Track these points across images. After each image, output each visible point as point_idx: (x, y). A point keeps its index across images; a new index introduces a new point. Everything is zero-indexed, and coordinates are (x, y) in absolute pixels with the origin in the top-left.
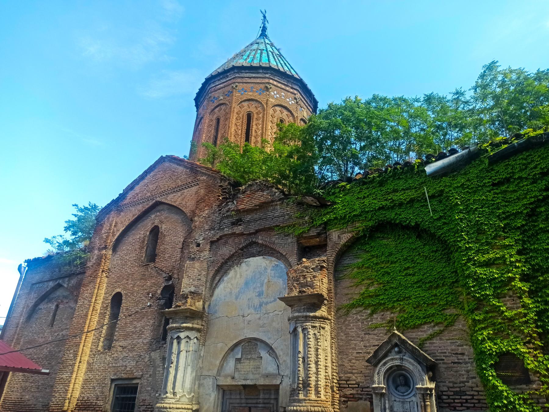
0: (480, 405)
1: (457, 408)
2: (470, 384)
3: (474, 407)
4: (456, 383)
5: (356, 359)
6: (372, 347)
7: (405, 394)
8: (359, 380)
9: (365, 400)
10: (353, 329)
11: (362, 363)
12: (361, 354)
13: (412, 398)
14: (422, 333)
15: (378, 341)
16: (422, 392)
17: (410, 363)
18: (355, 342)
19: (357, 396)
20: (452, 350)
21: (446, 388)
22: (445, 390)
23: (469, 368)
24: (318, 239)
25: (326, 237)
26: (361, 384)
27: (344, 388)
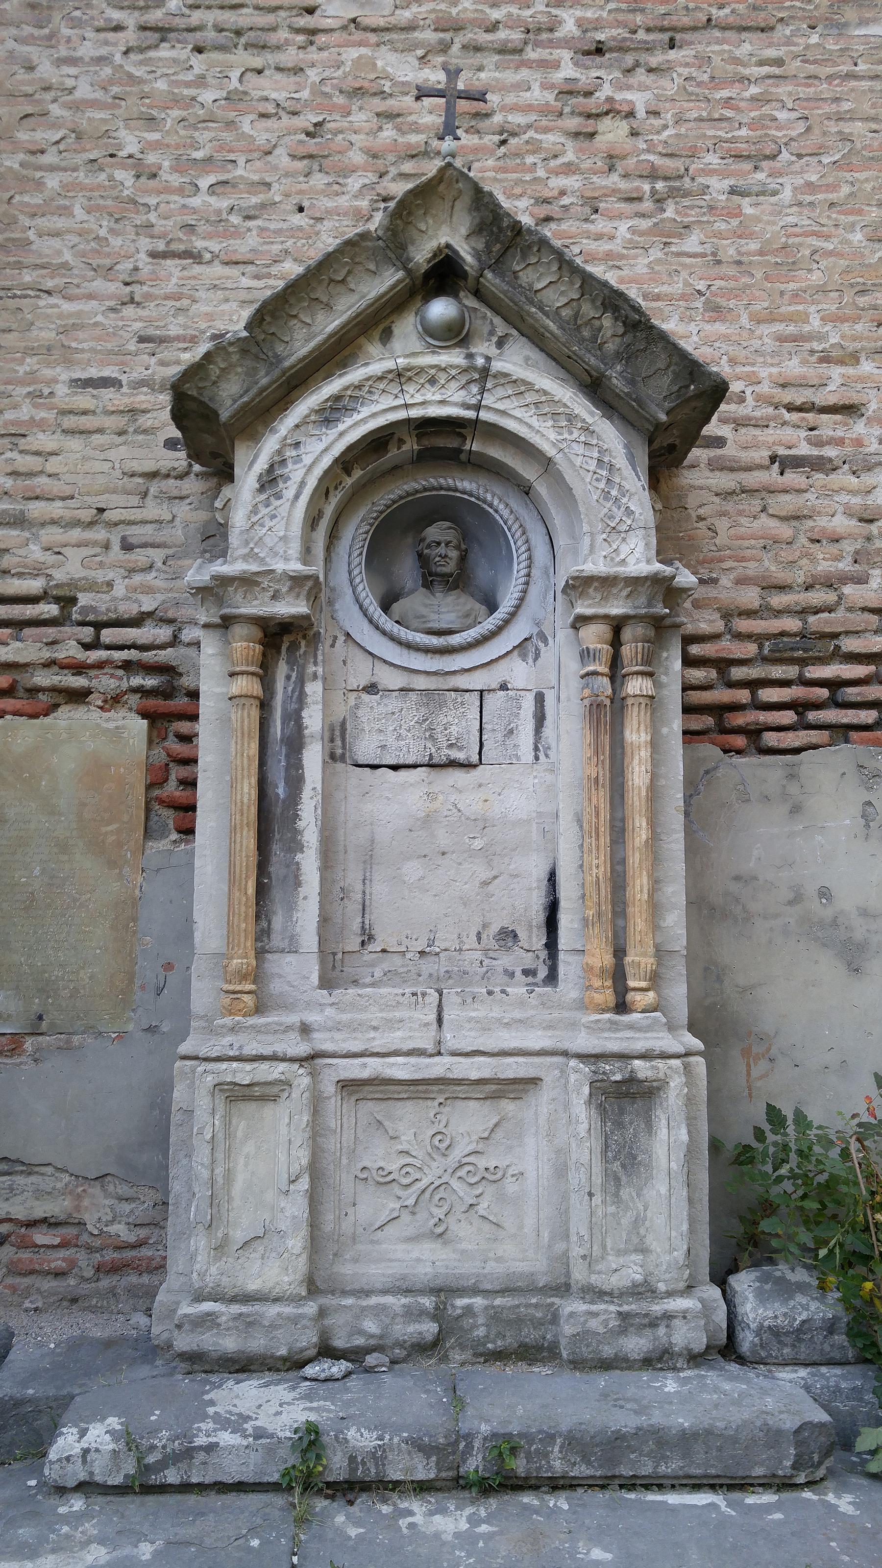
1: (771, 739)
4: (782, 588)
5: (70, 422)
7: (456, 640)
9: (114, 701)
10: (66, 211)
11: (112, 454)
12: (108, 394)
13: (503, 664)
18: (67, 307)
19: (43, 679)
20: (784, 386)
21: (717, 616)
22: (704, 627)
26: (84, 599)
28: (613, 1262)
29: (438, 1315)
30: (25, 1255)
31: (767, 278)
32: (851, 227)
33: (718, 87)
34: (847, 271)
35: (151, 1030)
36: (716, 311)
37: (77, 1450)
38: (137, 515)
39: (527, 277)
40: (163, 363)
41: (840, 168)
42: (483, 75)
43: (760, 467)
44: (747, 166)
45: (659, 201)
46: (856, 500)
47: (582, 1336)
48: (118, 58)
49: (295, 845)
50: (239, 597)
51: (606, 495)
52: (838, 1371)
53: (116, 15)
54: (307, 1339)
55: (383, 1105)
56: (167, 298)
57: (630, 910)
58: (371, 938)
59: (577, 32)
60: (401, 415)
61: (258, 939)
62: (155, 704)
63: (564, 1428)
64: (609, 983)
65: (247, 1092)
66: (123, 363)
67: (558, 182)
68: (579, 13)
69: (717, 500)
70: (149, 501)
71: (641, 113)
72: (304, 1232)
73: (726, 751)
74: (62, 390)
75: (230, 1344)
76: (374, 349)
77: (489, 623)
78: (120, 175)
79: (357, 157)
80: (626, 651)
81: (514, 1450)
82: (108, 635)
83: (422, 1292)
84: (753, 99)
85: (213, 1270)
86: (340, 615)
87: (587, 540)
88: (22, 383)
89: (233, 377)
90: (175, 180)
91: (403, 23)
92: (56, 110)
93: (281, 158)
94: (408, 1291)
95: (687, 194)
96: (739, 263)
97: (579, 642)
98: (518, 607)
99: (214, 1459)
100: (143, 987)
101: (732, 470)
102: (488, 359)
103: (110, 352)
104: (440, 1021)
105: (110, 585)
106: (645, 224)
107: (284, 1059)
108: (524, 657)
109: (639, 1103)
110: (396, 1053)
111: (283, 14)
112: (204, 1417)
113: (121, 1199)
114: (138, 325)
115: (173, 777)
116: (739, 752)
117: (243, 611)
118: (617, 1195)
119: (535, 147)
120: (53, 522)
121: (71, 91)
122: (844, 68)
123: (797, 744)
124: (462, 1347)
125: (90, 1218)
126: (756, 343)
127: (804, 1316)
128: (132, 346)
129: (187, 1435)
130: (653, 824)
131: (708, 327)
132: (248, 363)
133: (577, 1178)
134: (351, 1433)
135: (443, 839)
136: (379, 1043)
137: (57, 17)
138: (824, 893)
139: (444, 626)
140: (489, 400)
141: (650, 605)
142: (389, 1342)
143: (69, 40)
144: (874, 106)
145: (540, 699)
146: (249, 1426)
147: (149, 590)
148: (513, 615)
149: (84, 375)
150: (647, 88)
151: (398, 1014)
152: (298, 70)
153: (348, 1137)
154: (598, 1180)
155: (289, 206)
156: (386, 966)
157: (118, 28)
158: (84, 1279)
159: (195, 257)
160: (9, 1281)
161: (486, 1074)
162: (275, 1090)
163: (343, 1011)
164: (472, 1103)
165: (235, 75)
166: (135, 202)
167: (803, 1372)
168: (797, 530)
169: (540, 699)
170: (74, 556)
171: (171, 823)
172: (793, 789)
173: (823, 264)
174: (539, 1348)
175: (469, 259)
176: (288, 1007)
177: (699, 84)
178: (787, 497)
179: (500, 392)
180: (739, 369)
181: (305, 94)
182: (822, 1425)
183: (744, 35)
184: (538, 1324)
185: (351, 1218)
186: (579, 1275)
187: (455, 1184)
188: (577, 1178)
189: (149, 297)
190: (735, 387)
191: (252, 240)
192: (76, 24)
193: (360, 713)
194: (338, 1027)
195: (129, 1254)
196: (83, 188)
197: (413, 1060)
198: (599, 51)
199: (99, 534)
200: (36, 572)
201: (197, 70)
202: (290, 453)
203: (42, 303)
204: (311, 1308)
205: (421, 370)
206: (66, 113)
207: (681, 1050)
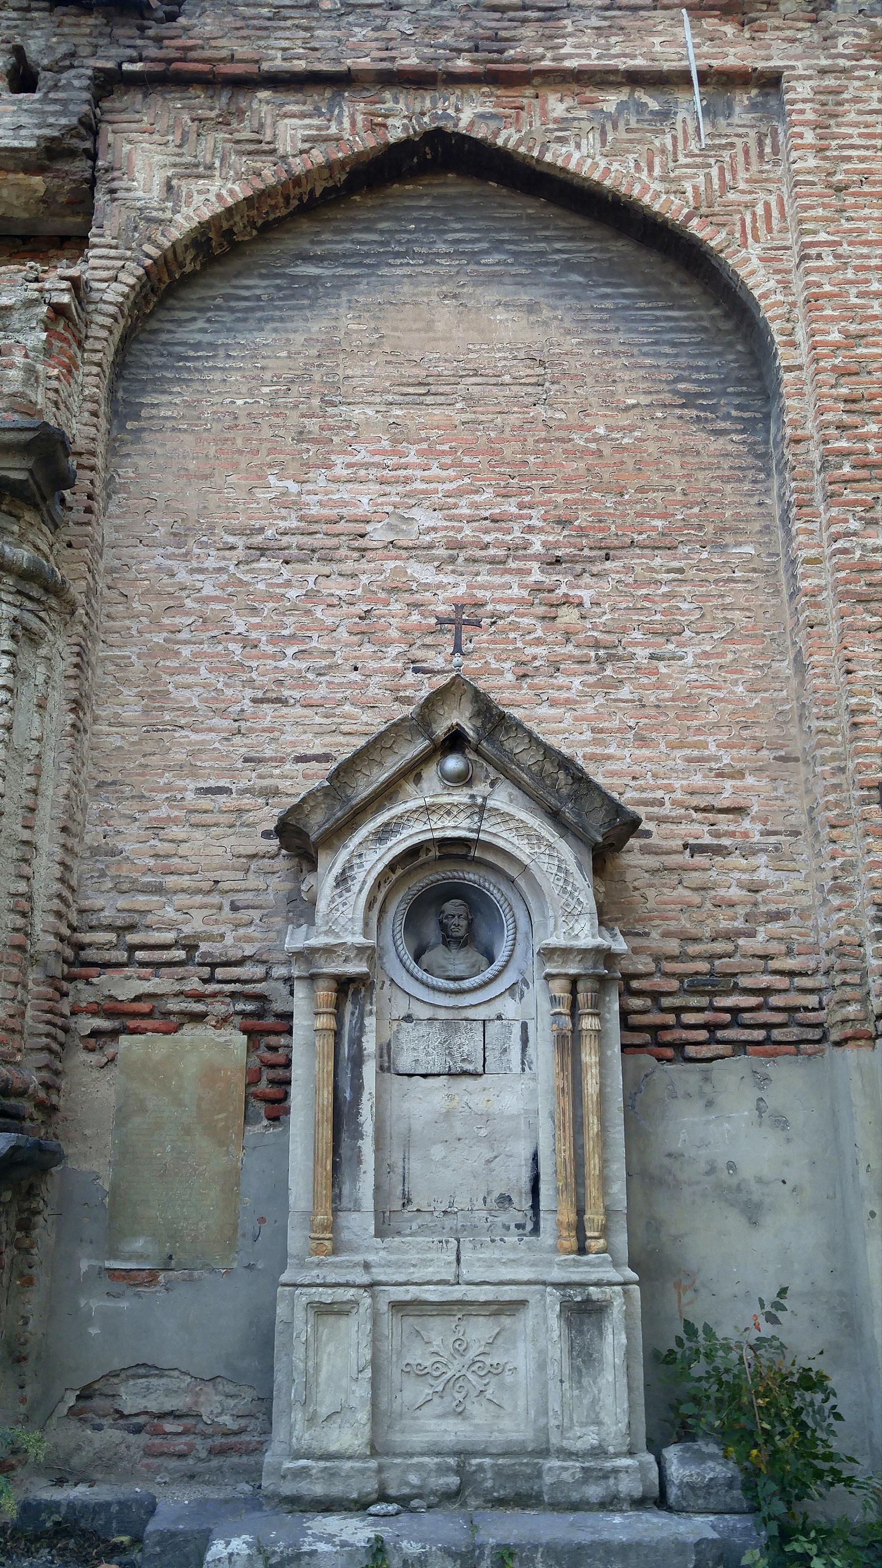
0: (793, 1033)
1: (691, 1051)
2: (758, 943)
3: (767, 1040)
4: (695, 940)
5: (195, 818)
6: (288, 766)
7: (466, 984)
8: (195, 925)
9: (223, 1021)
10: (195, 671)
11: (225, 842)
12: (222, 798)
13: (498, 1002)
14: (553, 711)
15: (328, 739)
16: (572, 971)
17: (522, 830)
18: (194, 737)
19: (173, 1005)
20: (692, 794)
21: (650, 960)
22: (641, 968)
23: (762, 874)
24: (37, 181)
25: (92, 182)
26: (204, 947)
27: (107, 965)
28: (578, 1431)
29: (459, 1471)
30: (157, 1441)
31: (678, 717)
32: (735, 683)
33: (639, 587)
34: (733, 713)
35: (250, 1267)
36: (642, 741)
37: (225, 1554)
38: (243, 885)
39: (509, 744)
40: (260, 777)
41: (726, 642)
42: (479, 578)
43: (676, 852)
44: (661, 640)
45: (601, 664)
46: (745, 877)
47: (558, 1484)
48: (232, 568)
49: (358, 1135)
50: (322, 961)
51: (564, 890)
52: (736, 1517)
53: (231, 539)
54: (371, 1486)
55: (420, 1320)
56: (264, 730)
57: (587, 1182)
58: (409, 1201)
59: (543, 551)
60: (429, 836)
61: (333, 1201)
62: (251, 1022)
63: (544, 1541)
64: (573, 1233)
65: (329, 1308)
66: (233, 777)
67: (531, 651)
68: (543, 538)
69: (646, 875)
70: (251, 875)
71: (587, 605)
72: (368, 1408)
73: (659, 1060)
74: (190, 796)
75: (319, 1489)
76: (410, 788)
77: (489, 973)
78: (232, 646)
79: (394, 634)
80: (581, 997)
81: (511, 1555)
82: (220, 973)
83: (448, 1454)
84: (664, 595)
85: (307, 1436)
86: (387, 966)
87: (552, 922)
88: (162, 790)
89: (319, 811)
90: (270, 649)
91: (425, 544)
92: (189, 603)
93: (342, 633)
94: (438, 1454)
95: (620, 659)
96: (658, 706)
97: (549, 991)
98: (508, 962)
99: (314, 1561)
100: (244, 1235)
101: (656, 854)
102: (485, 799)
103: (224, 769)
104: (458, 1260)
105: (222, 936)
106: (592, 679)
107: (353, 1286)
108: (513, 996)
109: (594, 1317)
110: (428, 1283)
111: (343, 538)
112: (306, 1535)
113: (228, 1396)
114: (243, 750)
115: (264, 1078)
116: (669, 1060)
117: (325, 970)
118: (579, 1382)
119: (515, 627)
120: (183, 891)
121: (199, 590)
122: (726, 575)
123: (709, 1055)
124: (477, 1495)
125: (204, 1411)
126: (671, 763)
127: (711, 1475)
128: (239, 765)
129: (296, 1545)
130: (602, 1120)
131: (637, 752)
132: (329, 801)
133: (552, 1370)
134: (404, 1544)
135: (459, 1129)
136: (418, 1275)
137: (191, 542)
138: (731, 1166)
139: (458, 974)
140: (485, 826)
141: (595, 967)
142: (426, 1491)
143: (199, 557)
144: (747, 600)
145: (524, 1026)
146: (336, 1540)
147: (249, 940)
148: (504, 967)
149: (205, 785)
150: (591, 587)
151: (429, 1256)
152: (353, 576)
153: (396, 1342)
154: (566, 1371)
155: (348, 666)
156: (419, 1221)
157: (232, 548)
158: (200, 1460)
159: (282, 701)
160: (145, 1461)
161: (491, 1297)
162: (348, 1307)
163: (392, 1253)
164: (481, 1319)
165: (311, 579)
166: (242, 665)
167: (712, 1518)
168: (704, 899)
169: (524, 1026)
170: (198, 916)
171: (263, 1112)
172: (707, 1089)
173: (716, 708)
174: (529, 1496)
175: (471, 733)
176: (355, 1250)
177: (626, 585)
178: (696, 874)
179: (493, 820)
180: (660, 782)
181: (359, 592)
182: (714, 1541)
183: (656, 552)
184: (528, 1478)
185: (399, 1400)
186: (555, 1440)
187: (470, 1376)
188: (552, 1370)
189: (251, 730)
190: (645, 826)
191: (323, 691)
192: (203, 545)
193: (400, 1036)
194: (388, 1264)
195: (233, 1440)
196: (206, 655)
197: (440, 1288)
198: (558, 561)
199: (215, 899)
200: (171, 926)
201: (285, 577)
202: (356, 861)
203: (177, 735)
204: (373, 1464)
205: (441, 806)
206: (196, 605)
207: (620, 1279)
